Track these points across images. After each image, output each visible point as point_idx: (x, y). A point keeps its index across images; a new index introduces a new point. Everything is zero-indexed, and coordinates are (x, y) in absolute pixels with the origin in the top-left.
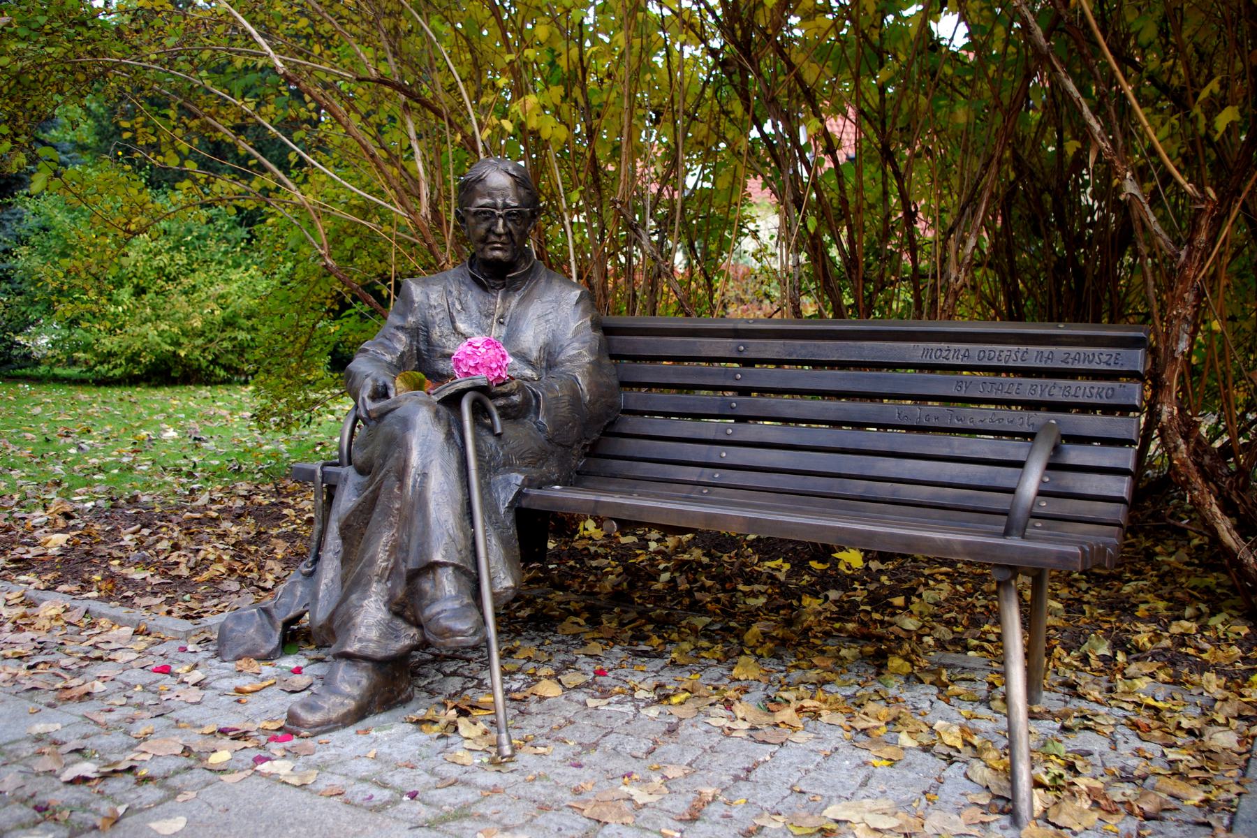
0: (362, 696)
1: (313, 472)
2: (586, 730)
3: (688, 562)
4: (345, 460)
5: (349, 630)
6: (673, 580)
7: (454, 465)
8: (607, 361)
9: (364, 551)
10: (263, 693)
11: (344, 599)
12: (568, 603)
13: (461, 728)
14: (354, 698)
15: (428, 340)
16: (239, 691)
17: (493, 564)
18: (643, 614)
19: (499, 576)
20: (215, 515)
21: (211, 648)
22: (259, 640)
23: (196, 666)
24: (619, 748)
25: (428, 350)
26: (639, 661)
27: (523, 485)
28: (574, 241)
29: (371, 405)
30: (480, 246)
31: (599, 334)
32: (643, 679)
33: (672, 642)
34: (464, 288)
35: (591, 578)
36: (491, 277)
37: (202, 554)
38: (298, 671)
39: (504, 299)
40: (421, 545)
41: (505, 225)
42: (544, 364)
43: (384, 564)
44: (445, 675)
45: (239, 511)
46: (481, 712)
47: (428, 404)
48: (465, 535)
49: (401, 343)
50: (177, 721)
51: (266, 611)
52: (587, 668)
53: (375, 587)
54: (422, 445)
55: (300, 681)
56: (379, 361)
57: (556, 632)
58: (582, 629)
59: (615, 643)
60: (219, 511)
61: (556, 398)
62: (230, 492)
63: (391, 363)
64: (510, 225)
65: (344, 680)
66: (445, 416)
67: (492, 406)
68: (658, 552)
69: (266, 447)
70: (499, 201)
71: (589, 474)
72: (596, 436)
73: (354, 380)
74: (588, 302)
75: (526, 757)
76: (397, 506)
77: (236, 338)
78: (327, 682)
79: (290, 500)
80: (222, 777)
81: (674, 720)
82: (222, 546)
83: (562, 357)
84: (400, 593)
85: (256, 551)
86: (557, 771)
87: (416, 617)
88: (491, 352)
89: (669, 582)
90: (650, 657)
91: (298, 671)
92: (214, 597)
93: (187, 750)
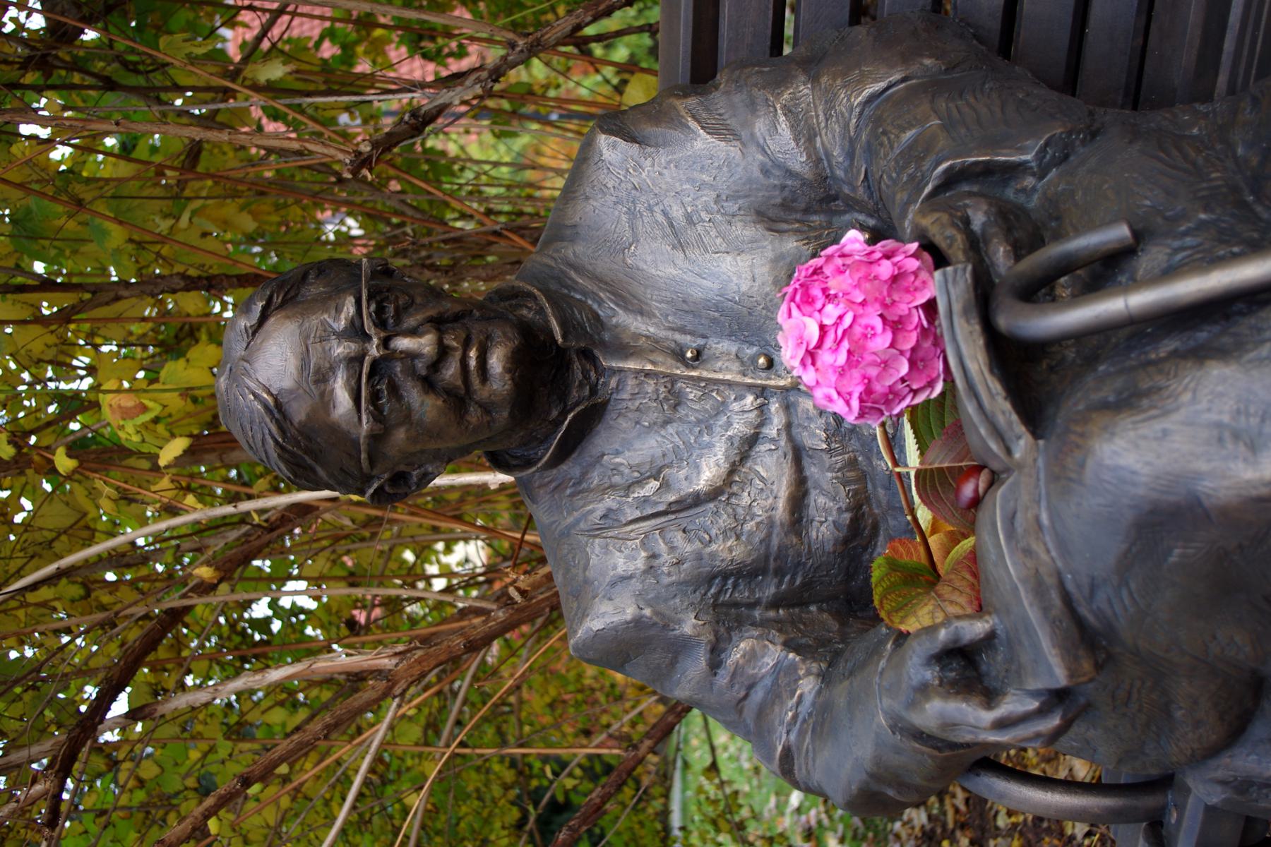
15: (747, 573)
25: (779, 573)
34: (595, 478)
36: (563, 398)
39: (624, 350)
41: (413, 332)
42: (817, 219)
63: (825, 678)
64: (411, 322)
70: (340, 349)
83: (798, 161)
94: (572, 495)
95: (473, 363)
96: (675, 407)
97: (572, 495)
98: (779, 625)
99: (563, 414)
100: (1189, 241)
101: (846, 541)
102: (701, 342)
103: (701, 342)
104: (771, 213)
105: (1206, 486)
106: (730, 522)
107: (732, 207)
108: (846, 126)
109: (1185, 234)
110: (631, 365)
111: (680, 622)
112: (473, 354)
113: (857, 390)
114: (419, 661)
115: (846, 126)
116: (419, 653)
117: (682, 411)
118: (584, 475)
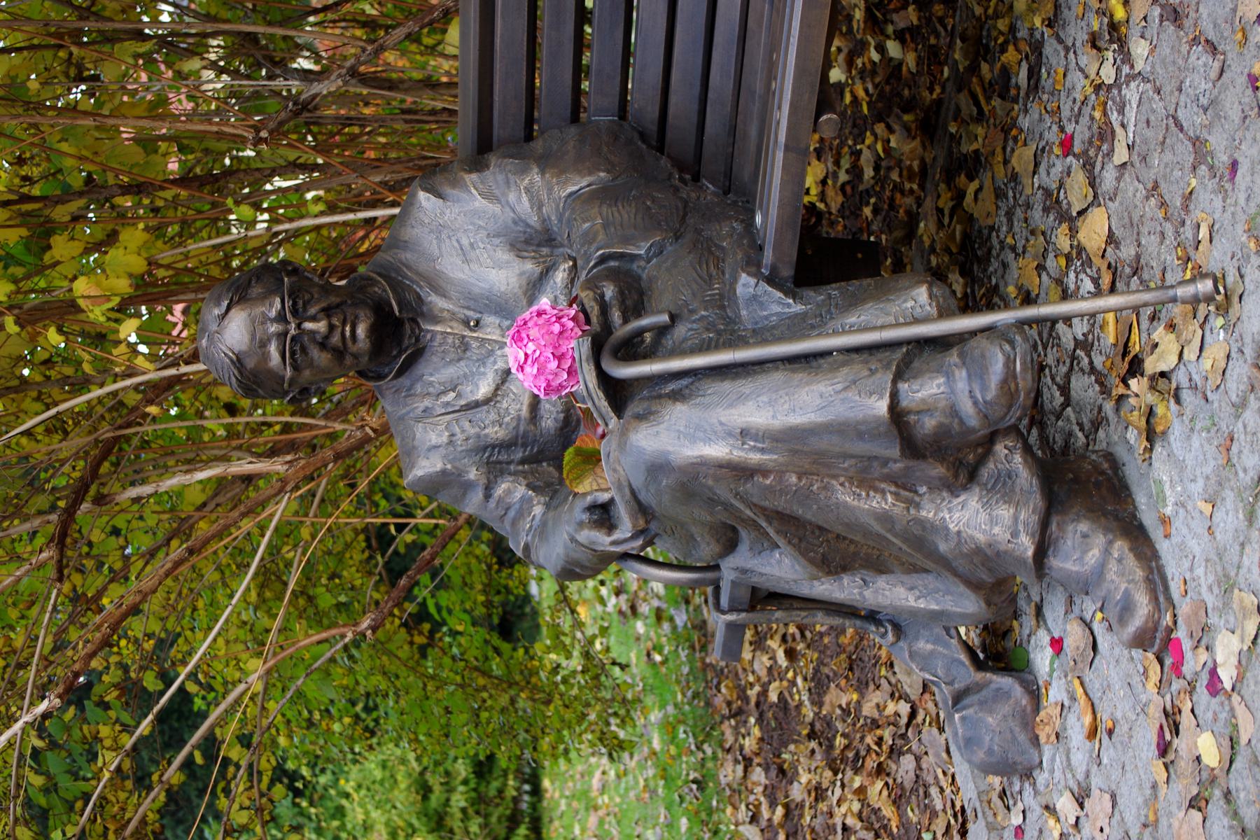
0: (1107, 530)
1: (730, 626)
2: (1171, 163)
3: (868, 10)
4: (709, 575)
5: (998, 554)
6: (900, 36)
7: (727, 386)
8: (538, 145)
9: (867, 533)
10: (1096, 696)
11: (944, 564)
12: (940, 211)
13: (1163, 367)
14: (1111, 543)
16: (1093, 733)
17: (891, 320)
18: (961, 83)
19: (912, 309)
20: (780, 811)
21: (1017, 788)
22: (1006, 709)
23: (1049, 809)
24: (1204, 101)
25: (524, 445)
26: (1046, 82)
27: (757, 275)
28: (322, 213)
29: (625, 529)
30: (349, 360)
31: (493, 159)
32: (1078, 70)
33: (1013, 29)
34: (418, 388)
35: (895, 176)
36: (400, 343)
37: (850, 821)
38: (1057, 644)
39: (436, 320)
40: (860, 435)
41: (314, 319)
42: (545, 251)
43: (890, 499)
44: (1067, 403)
45: (773, 773)
46: (1135, 337)
47: (624, 433)
48: (844, 364)
49: (512, 490)
50: (1145, 826)
51: (958, 698)
52: (1059, 168)
53: (928, 513)
54: (693, 440)
55: (1074, 637)
56: (544, 524)
57: (992, 228)
58: (988, 183)
59: (1014, 124)
60: (773, 805)
61: (605, 226)
62: (737, 792)
63: (548, 506)
64: (312, 311)
65: (1081, 559)
66: (645, 404)
67: (622, 330)
68: (850, 63)
69: (656, 744)
70: (273, 328)
71: (729, 174)
72: (664, 162)
73: (578, 563)
74: (439, 179)
75: (1215, 257)
76: (794, 479)
77: (464, 810)
78: (1084, 586)
79: (753, 693)
80: (1244, 740)
81: (1157, 11)
82: (838, 791)
83: (534, 220)
84: (938, 470)
85: (844, 735)
86: (1242, 202)
87: (978, 445)
88: (534, 333)
89: (903, 42)
90: (1039, 64)
91: (1057, 644)
92: (927, 795)
93: (1194, 803)
94: (405, 397)
95: (348, 334)
96: (465, 351)
97: (405, 397)
98: (524, 474)
99: (399, 355)
100: (695, 326)
101: (562, 429)
102: (479, 315)
103: (479, 315)
104: (518, 246)
105: (672, 457)
106: (496, 417)
107: (497, 241)
108: (558, 206)
109: (694, 322)
110: (438, 328)
111: (467, 472)
112: (348, 329)
113: (544, 385)
114: (303, 468)
115: (558, 206)
116: (303, 462)
117: (468, 354)
118: (412, 385)
